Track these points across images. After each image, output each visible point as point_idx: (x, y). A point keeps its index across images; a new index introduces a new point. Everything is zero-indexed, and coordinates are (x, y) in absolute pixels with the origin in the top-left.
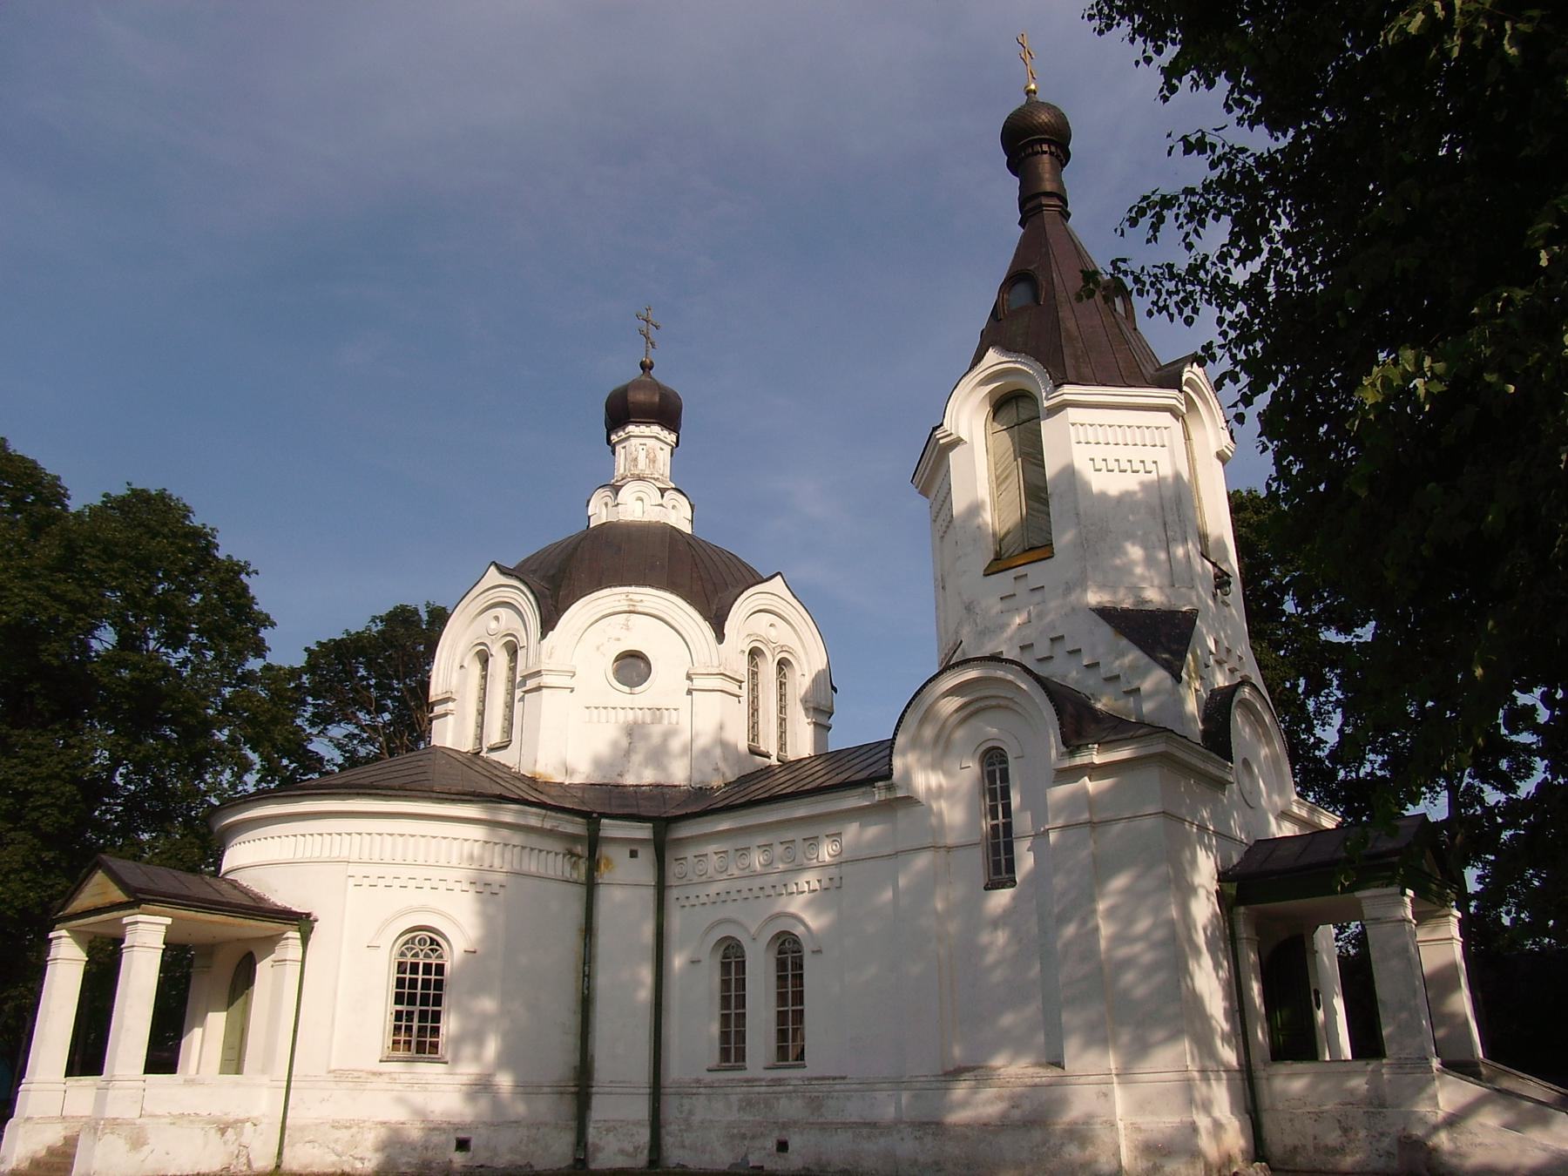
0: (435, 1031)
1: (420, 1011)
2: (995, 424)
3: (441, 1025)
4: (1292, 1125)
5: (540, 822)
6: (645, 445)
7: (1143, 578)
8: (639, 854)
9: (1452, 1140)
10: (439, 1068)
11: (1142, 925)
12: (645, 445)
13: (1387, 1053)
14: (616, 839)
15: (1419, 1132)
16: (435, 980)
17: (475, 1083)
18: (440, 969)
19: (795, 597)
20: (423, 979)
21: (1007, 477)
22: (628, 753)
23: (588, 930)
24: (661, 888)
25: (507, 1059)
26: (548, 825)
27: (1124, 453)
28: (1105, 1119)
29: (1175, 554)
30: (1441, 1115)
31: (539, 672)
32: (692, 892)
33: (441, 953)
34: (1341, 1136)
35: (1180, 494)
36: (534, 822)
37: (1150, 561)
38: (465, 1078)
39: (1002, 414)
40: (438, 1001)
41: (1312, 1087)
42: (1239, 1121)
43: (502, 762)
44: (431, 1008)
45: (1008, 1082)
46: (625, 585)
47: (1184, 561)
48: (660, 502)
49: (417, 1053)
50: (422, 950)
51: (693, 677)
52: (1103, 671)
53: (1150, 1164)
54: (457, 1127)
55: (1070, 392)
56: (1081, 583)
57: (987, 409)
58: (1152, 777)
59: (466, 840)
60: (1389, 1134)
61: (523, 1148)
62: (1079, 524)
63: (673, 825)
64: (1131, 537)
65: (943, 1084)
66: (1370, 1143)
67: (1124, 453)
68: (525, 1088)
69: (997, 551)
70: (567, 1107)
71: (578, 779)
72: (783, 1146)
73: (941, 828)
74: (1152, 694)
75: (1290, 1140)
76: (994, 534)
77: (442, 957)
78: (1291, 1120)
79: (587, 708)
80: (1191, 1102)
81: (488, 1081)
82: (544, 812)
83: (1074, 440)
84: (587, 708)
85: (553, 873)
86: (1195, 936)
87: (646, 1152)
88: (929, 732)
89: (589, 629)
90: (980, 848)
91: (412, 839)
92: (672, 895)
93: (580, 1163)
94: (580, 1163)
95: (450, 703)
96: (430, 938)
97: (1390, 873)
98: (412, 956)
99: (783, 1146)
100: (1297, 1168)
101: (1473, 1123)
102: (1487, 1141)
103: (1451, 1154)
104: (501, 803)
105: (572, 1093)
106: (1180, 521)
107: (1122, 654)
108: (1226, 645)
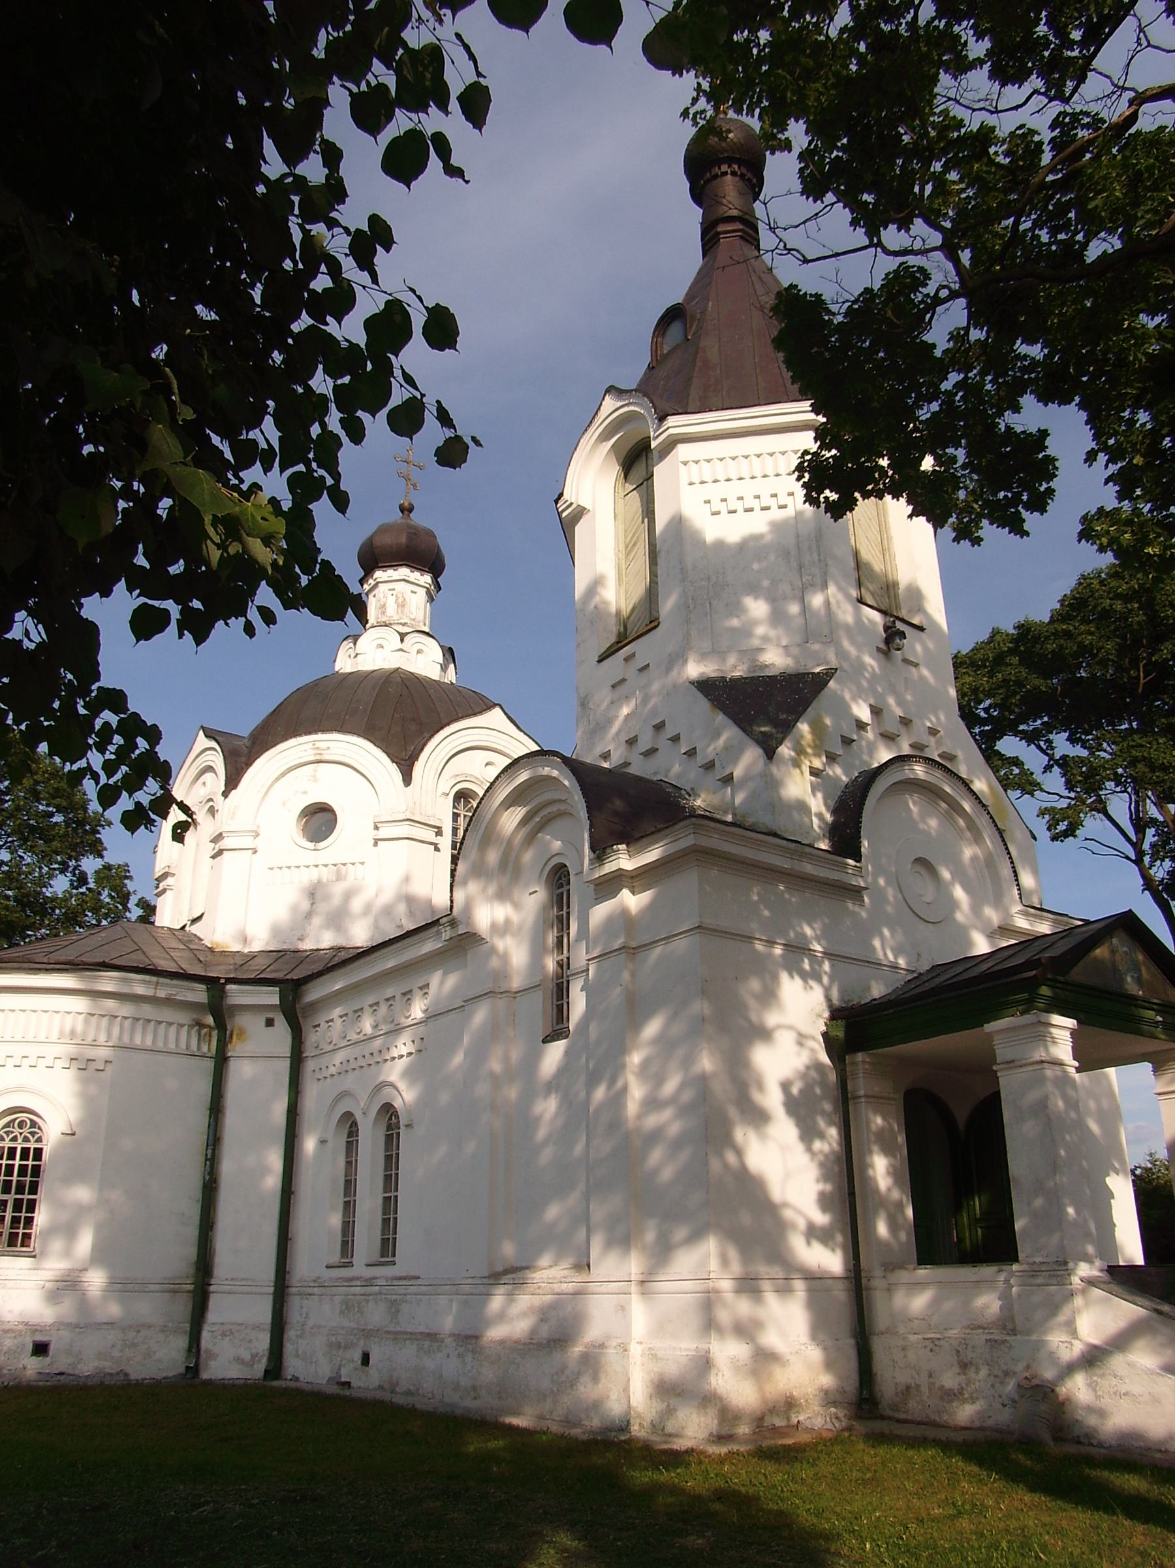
0: (29, 1222)
1: (15, 1199)
2: (627, 485)
3: (35, 1215)
4: (905, 1356)
5: (153, 991)
6: (394, 589)
7: (766, 639)
8: (276, 1023)
9: (1092, 1386)
10: (25, 1262)
11: (671, 1086)
12: (394, 589)
13: (1021, 1256)
14: (244, 1005)
15: (1049, 1374)
16: (33, 1165)
17: (58, 1279)
18: (38, 1153)
19: (521, 730)
20: (20, 1165)
21: (634, 545)
22: (309, 915)
23: (216, 1108)
24: (297, 1060)
25: (101, 1255)
26: (162, 993)
27: (748, 489)
28: (620, 1341)
29: (809, 602)
30: (1078, 1348)
31: (221, 834)
32: (324, 1061)
33: (40, 1137)
34: (959, 1374)
35: (820, 529)
36: (140, 990)
37: (777, 617)
38: (52, 1273)
39: (631, 476)
40: (34, 1189)
41: (935, 1303)
42: (825, 1349)
43: (198, 935)
44: (26, 1197)
45: (539, 1288)
46: (310, 733)
47: (823, 612)
48: (400, 646)
49: (8, 1246)
50: (21, 1134)
51: (379, 825)
52: (700, 759)
53: (664, 1405)
54: (34, 1329)
55: (677, 424)
56: (678, 658)
57: (615, 469)
58: (689, 881)
59: (69, 1013)
60: (1015, 1373)
61: (116, 1353)
62: (683, 580)
63: (304, 988)
64: (754, 590)
65: (482, 1289)
66: (993, 1386)
67: (748, 489)
68: (120, 1286)
69: (619, 633)
70: (182, 1308)
71: (256, 947)
72: (366, 1359)
73: (503, 973)
74: (746, 779)
75: (903, 1377)
76: (618, 613)
77: (41, 1141)
78: (904, 1349)
79: (271, 869)
80: (709, 1324)
81: (79, 1277)
82: (154, 979)
83: (684, 481)
84: (271, 869)
85: (139, 1043)
86: (756, 1096)
87: (265, 1360)
88: (493, 856)
89: (276, 785)
90: (541, 993)
91: (46, 1015)
92: (310, 1066)
93: (193, 1371)
94: (193, 1371)
95: (169, 878)
96: (31, 1120)
97: (1025, 995)
98: (11, 1140)
99: (366, 1359)
100: (910, 1417)
101: (1118, 1362)
102: (1136, 1389)
103: (1090, 1409)
104: (100, 971)
105: (189, 1292)
106: (820, 561)
107: (717, 735)
108: (899, 712)
